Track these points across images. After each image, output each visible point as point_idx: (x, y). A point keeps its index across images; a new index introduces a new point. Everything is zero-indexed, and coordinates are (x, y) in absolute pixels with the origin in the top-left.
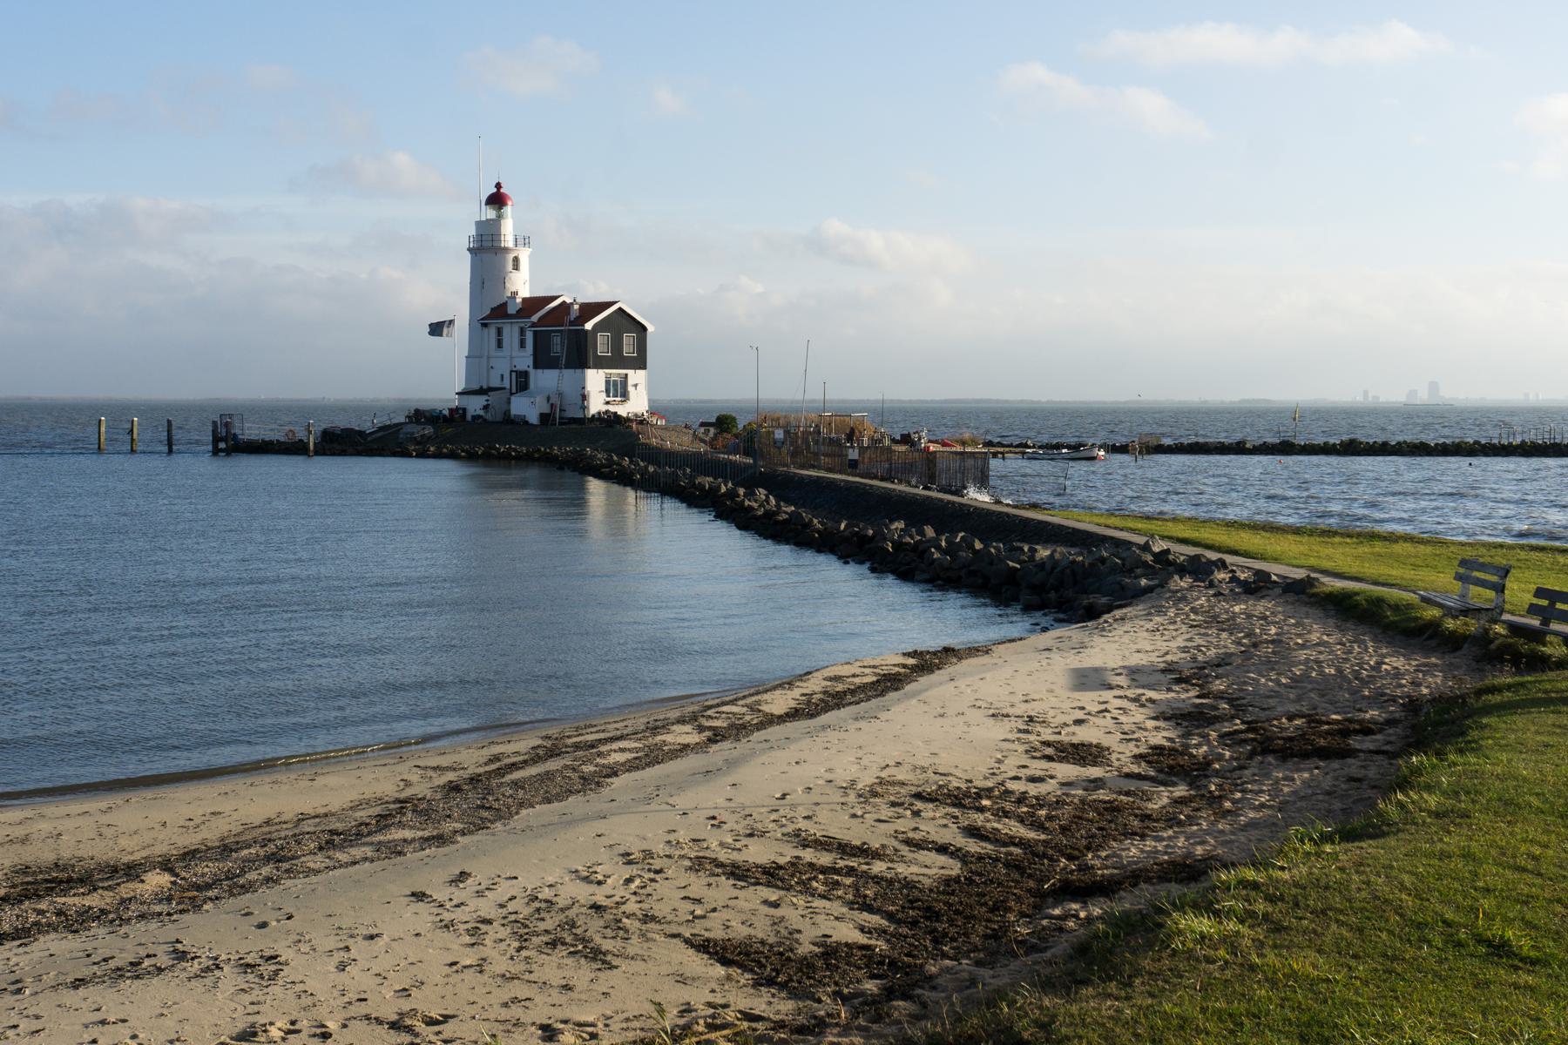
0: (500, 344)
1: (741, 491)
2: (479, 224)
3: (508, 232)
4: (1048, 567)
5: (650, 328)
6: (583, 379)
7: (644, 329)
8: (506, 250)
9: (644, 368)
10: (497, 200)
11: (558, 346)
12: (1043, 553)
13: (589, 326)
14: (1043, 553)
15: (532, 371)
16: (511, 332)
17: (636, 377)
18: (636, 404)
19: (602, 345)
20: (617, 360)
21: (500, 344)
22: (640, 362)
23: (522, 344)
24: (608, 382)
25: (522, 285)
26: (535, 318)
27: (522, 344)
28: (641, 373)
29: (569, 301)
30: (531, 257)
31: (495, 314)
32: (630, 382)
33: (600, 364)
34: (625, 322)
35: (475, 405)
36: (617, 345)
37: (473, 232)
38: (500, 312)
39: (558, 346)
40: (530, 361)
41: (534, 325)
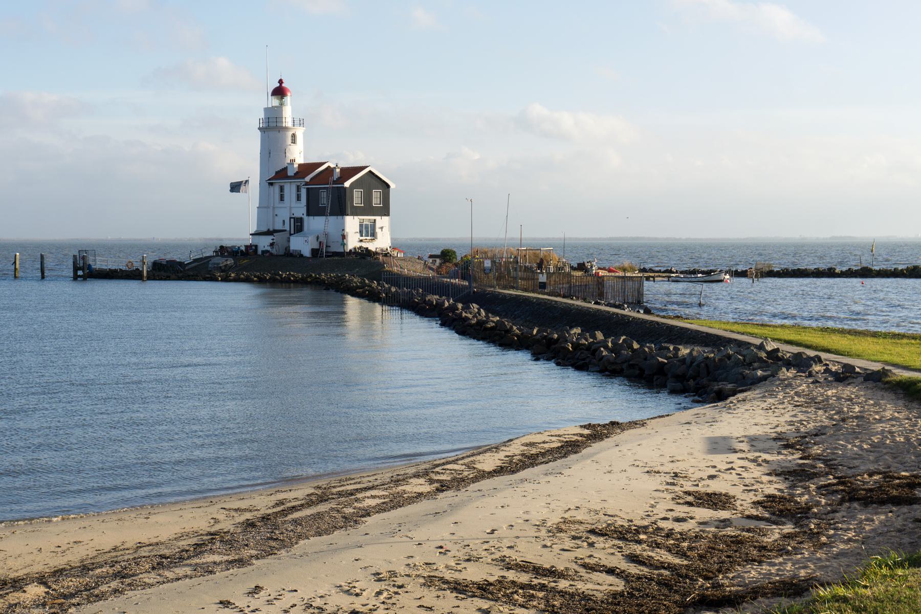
0: (282, 198)
1: (460, 306)
2: (267, 110)
3: (288, 115)
4: (688, 361)
5: (392, 186)
6: (343, 224)
7: (388, 186)
8: (286, 128)
9: (388, 215)
10: (280, 92)
11: (324, 199)
12: (684, 351)
13: (347, 184)
14: (684, 351)
15: (305, 218)
16: (290, 189)
17: (382, 222)
18: (382, 242)
19: (357, 198)
20: (368, 209)
21: (282, 198)
22: (385, 211)
23: (299, 198)
24: (361, 226)
25: (298, 155)
26: (308, 179)
27: (299, 198)
28: (386, 218)
29: (332, 166)
30: (304, 134)
31: (278, 177)
32: (378, 225)
33: (356, 212)
34: (374, 181)
35: (264, 243)
36: (368, 198)
37: (262, 116)
38: (282, 174)
39: (324, 199)
40: (304, 210)
41: (307, 184)
